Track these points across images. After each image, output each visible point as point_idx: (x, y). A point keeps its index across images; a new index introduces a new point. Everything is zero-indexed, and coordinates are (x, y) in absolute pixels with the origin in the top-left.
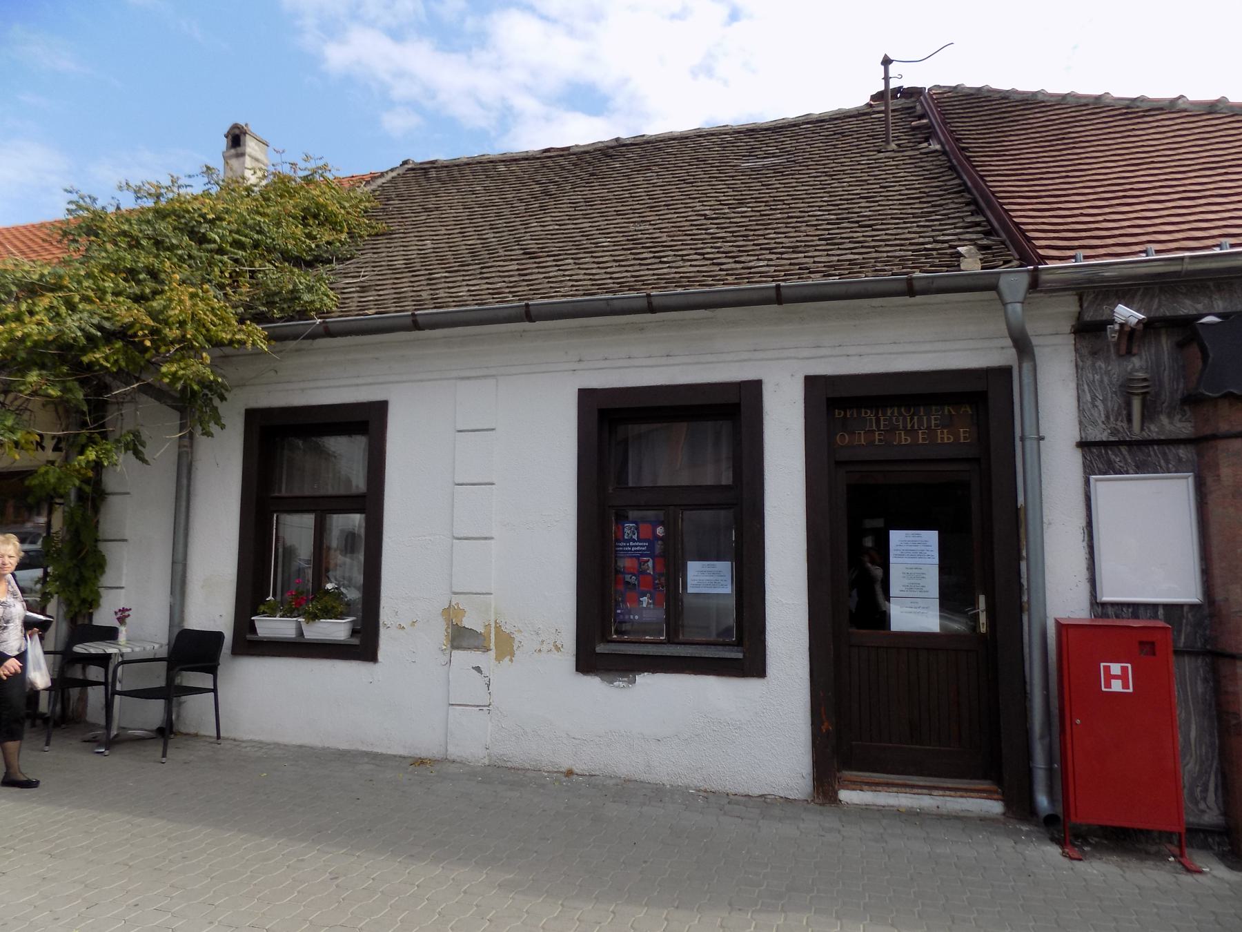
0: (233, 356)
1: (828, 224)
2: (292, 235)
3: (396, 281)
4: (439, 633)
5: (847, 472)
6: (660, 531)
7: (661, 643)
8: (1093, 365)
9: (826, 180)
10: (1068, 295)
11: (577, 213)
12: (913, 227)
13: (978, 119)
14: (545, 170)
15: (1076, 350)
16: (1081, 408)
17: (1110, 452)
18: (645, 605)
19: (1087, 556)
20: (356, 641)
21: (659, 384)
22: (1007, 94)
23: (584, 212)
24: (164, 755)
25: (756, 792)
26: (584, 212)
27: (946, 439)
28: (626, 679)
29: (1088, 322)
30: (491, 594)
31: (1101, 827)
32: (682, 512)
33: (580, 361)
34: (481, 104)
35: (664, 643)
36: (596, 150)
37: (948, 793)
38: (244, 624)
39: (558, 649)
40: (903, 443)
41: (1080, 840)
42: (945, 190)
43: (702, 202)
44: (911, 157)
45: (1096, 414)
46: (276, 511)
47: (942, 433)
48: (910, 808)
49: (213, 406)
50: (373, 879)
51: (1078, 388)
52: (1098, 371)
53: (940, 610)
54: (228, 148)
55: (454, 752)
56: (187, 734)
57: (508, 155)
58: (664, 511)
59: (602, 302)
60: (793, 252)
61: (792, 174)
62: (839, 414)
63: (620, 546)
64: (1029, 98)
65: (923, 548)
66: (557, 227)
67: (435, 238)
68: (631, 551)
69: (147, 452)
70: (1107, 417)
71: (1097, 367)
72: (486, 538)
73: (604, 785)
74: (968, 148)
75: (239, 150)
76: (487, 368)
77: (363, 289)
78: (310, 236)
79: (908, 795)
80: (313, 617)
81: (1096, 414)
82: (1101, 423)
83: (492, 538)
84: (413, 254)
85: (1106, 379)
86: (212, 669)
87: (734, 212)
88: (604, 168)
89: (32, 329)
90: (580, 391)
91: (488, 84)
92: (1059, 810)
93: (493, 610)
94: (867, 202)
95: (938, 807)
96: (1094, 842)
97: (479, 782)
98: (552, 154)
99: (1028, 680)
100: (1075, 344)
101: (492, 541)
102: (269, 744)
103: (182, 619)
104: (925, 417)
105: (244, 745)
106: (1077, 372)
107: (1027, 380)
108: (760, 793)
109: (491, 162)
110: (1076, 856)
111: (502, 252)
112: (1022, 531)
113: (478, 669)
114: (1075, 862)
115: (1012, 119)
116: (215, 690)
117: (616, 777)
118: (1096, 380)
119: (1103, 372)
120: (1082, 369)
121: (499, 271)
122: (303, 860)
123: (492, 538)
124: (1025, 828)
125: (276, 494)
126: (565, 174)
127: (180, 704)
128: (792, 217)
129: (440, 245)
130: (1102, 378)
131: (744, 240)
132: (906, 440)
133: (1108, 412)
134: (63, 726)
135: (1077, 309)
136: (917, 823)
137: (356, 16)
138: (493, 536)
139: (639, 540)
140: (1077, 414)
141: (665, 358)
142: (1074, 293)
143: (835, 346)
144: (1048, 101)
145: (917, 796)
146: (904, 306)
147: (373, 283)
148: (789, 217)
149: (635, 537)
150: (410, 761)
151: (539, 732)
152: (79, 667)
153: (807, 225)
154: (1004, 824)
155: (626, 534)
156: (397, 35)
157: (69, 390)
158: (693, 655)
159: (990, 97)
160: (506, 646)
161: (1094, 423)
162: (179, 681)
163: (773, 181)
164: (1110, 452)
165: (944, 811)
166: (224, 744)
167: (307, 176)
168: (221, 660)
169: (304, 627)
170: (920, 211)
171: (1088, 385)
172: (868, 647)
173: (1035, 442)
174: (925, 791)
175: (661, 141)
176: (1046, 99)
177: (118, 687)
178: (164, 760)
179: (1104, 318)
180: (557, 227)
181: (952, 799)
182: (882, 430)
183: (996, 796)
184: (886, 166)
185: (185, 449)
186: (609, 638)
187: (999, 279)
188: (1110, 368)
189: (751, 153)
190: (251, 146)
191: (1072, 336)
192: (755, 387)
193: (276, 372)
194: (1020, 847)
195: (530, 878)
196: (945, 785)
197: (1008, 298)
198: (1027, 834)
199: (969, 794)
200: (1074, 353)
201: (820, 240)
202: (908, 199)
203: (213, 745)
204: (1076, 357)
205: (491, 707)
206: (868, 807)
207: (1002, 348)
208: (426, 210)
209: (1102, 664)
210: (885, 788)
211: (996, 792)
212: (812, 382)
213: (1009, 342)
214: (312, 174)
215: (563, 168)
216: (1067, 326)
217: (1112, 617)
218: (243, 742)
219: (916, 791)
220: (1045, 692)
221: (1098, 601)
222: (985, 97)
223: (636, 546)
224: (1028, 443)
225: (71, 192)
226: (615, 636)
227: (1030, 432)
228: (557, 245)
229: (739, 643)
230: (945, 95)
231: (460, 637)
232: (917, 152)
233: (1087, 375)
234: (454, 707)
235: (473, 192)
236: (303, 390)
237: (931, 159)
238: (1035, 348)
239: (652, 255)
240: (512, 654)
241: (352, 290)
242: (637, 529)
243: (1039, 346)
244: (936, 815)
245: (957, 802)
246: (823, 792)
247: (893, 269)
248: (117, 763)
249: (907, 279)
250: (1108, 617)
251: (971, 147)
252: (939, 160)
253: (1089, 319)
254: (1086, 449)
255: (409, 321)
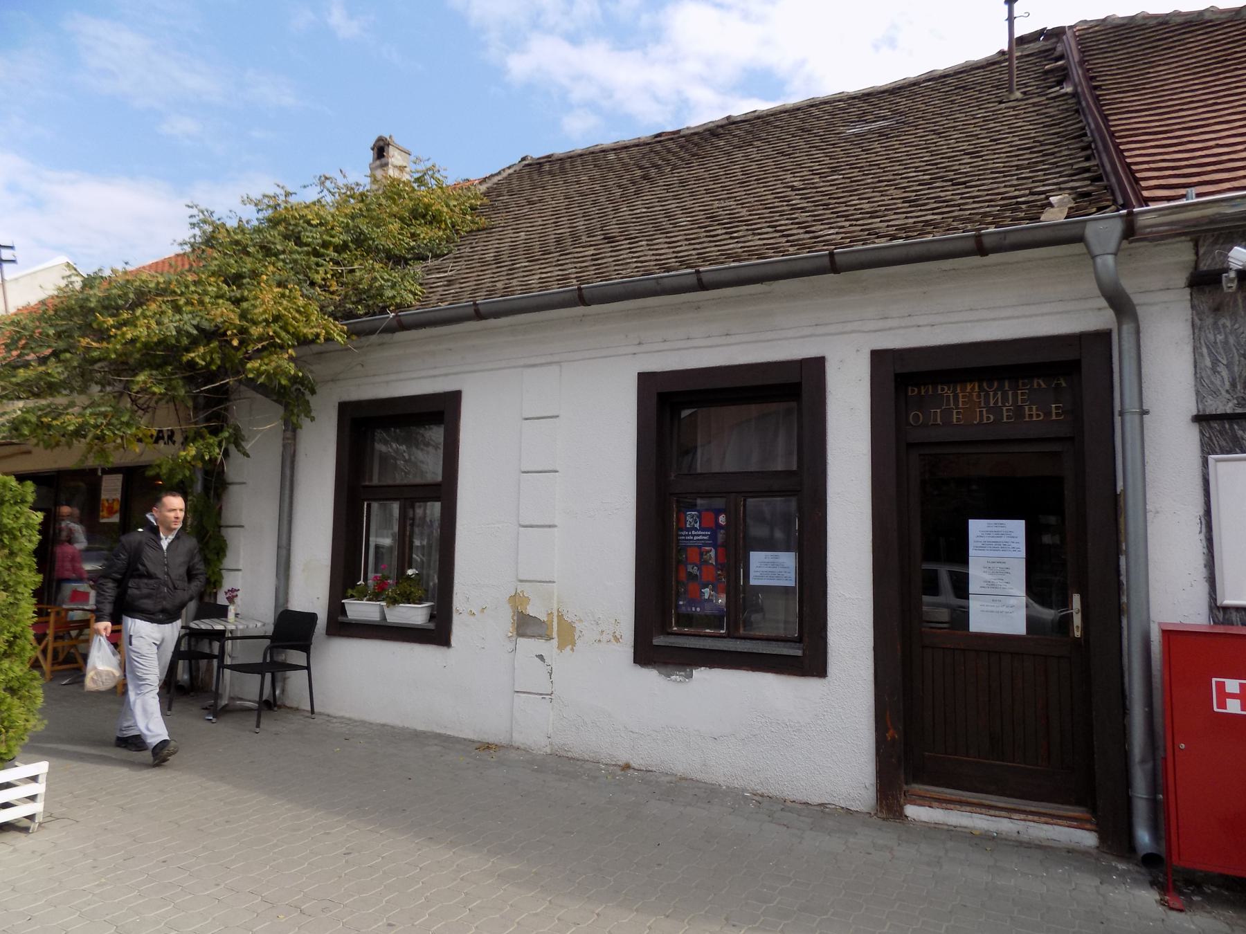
0: (327, 352)
1: (919, 185)
2: (391, 234)
3: (480, 273)
4: (506, 622)
5: (920, 455)
6: (722, 519)
7: (721, 637)
8: (1215, 323)
9: (933, 139)
10: (1181, 242)
11: (667, 195)
12: (1012, 180)
13: (1125, 51)
14: (652, 155)
15: (1193, 307)
16: (1198, 376)
17: (1236, 427)
18: (706, 597)
19: (1205, 551)
20: (432, 626)
21: (718, 365)
22: (1168, 18)
23: (675, 193)
24: (258, 726)
25: (816, 800)
26: (675, 193)
27: (1034, 416)
28: (683, 673)
29: (1205, 271)
30: (554, 582)
31: (1221, 875)
32: (745, 500)
33: (640, 344)
34: (656, 99)
35: (724, 637)
36: (706, 130)
37: (1030, 817)
38: (336, 609)
39: (617, 640)
40: (985, 422)
41: (1191, 888)
42: (1064, 136)
43: (794, 173)
44: (1034, 104)
45: (1218, 382)
46: (367, 500)
47: (1031, 409)
48: (986, 831)
49: (305, 400)
50: (383, 858)
51: (1194, 352)
52: (1222, 330)
53: (967, 613)
54: (374, 160)
55: (518, 739)
56: (289, 708)
57: (621, 143)
58: (724, 500)
59: (651, 281)
60: (870, 218)
61: (897, 136)
62: (912, 392)
63: (682, 535)
64: (1194, 20)
65: (1008, 540)
66: (644, 210)
67: (530, 229)
68: (693, 540)
69: (248, 446)
70: (1233, 385)
71: (1220, 326)
72: (550, 526)
73: (657, 782)
74: (1100, 86)
75: (383, 160)
76: (551, 354)
77: (450, 282)
78: (413, 236)
79: (983, 816)
80: (394, 601)
81: (1218, 382)
82: (1224, 393)
83: (555, 526)
84: (505, 246)
85: (1232, 340)
86: (306, 648)
87: (823, 182)
88: (708, 148)
89: (142, 332)
90: (639, 374)
91: (661, 77)
92: (1162, 850)
93: (555, 598)
94: (971, 158)
95: (1018, 832)
96: (1209, 891)
97: (534, 770)
98: (662, 138)
99: (1127, 693)
100: (1192, 299)
101: (556, 529)
102: (356, 721)
103: (287, 601)
104: (1010, 393)
105: (335, 720)
106: (1194, 333)
107: (1128, 344)
108: (820, 802)
109: (603, 151)
110: (1177, 906)
111: (584, 238)
112: (1122, 520)
113: (541, 657)
114: (1174, 914)
115: (1165, 46)
116: (308, 668)
117: (672, 774)
118: (1218, 341)
119: (1228, 331)
120: (1200, 329)
121: (575, 258)
122: (328, 833)
123: (555, 526)
124: (1122, 866)
125: (367, 483)
126: (670, 157)
127: (285, 679)
128: (882, 181)
129: (532, 236)
130: (1226, 337)
131: (824, 209)
132: (988, 418)
133: (1234, 379)
134: (192, 694)
135: (1192, 257)
136: (989, 849)
137: (537, 22)
138: (557, 524)
139: (702, 529)
140: (1193, 383)
141: (724, 337)
142: (1188, 238)
143: (904, 317)
144: (1217, 19)
145: (994, 818)
146: (978, 267)
147: (460, 277)
148: (879, 182)
149: (697, 526)
150: (477, 745)
151: (598, 724)
152: (206, 642)
153: (896, 189)
154: (1097, 859)
155: (688, 523)
156: (574, 39)
157: (174, 389)
158: (750, 651)
159: (1145, 24)
160: (568, 636)
161: (1215, 393)
162: (283, 658)
163: (876, 145)
164: (1236, 427)
165: (1024, 837)
166: (318, 720)
167: (420, 177)
168: (314, 640)
169: (386, 610)
170: (1027, 162)
171: (1208, 347)
172: (943, 648)
173: (1137, 418)
174: (1003, 813)
175: (772, 115)
176: (1214, 17)
177: (228, 661)
178: (258, 730)
179: (1218, 267)
180: (644, 210)
181: (1035, 824)
182: (961, 408)
183: (1088, 826)
184: (1004, 117)
185: (289, 441)
186: (669, 631)
187: (1085, 227)
188: (1236, 326)
189: (861, 119)
190: (395, 157)
191: (1188, 291)
192: (816, 366)
193: (362, 365)
194: (1104, 888)
195: (534, 870)
196: (1028, 809)
197: (1096, 249)
198: (1122, 874)
199: (1055, 821)
200: (1190, 311)
201: (903, 202)
202: (1018, 150)
203: (307, 719)
204: (1192, 314)
205: (553, 696)
206: (937, 826)
207: (1100, 309)
208: (531, 203)
209: (1214, 680)
210: (958, 806)
211: (1088, 821)
212: (879, 358)
213: (1103, 303)
214: (423, 176)
215: (669, 151)
216: (1181, 278)
217: (1237, 625)
218: (335, 718)
219: (992, 812)
220: (1147, 709)
221: (1218, 604)
222: (1138, 26)
223: (698, 535)
224: (1128, 417)
225: (192, 207)
226: (675, 629)
227: (1131, 404)
228: (637, 228)
229: (799, 640)
230: (1091, 31)
231: (525, 625)
232: (1044, 98)
233: (1206, 336)
234: (519, 694)
235: (578, 182)
236: (387, 382)
237: (1058, 104)
238: (1137, 308)
239: (724, 231)
240: (574, 644)
241: (439, 284)
242: (700, 517)
243: (1144, 304)
244: (1017, 841)
245: (1041, 828)
246: (887, 805)
247: (967, 227)
248: (224, 729)
249: (975, 235)
250: (1233, 624)
251: (1104, 85)
252: (1067, 104)
253: (1205, 268)
254: (1204, 424)
255: (471, 311)
